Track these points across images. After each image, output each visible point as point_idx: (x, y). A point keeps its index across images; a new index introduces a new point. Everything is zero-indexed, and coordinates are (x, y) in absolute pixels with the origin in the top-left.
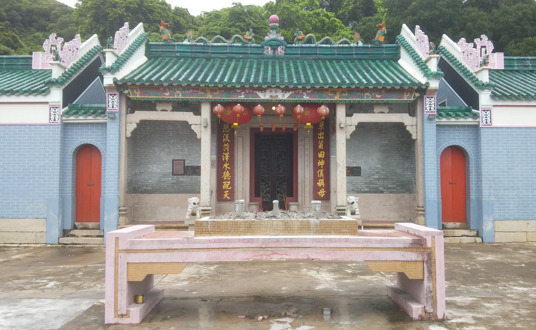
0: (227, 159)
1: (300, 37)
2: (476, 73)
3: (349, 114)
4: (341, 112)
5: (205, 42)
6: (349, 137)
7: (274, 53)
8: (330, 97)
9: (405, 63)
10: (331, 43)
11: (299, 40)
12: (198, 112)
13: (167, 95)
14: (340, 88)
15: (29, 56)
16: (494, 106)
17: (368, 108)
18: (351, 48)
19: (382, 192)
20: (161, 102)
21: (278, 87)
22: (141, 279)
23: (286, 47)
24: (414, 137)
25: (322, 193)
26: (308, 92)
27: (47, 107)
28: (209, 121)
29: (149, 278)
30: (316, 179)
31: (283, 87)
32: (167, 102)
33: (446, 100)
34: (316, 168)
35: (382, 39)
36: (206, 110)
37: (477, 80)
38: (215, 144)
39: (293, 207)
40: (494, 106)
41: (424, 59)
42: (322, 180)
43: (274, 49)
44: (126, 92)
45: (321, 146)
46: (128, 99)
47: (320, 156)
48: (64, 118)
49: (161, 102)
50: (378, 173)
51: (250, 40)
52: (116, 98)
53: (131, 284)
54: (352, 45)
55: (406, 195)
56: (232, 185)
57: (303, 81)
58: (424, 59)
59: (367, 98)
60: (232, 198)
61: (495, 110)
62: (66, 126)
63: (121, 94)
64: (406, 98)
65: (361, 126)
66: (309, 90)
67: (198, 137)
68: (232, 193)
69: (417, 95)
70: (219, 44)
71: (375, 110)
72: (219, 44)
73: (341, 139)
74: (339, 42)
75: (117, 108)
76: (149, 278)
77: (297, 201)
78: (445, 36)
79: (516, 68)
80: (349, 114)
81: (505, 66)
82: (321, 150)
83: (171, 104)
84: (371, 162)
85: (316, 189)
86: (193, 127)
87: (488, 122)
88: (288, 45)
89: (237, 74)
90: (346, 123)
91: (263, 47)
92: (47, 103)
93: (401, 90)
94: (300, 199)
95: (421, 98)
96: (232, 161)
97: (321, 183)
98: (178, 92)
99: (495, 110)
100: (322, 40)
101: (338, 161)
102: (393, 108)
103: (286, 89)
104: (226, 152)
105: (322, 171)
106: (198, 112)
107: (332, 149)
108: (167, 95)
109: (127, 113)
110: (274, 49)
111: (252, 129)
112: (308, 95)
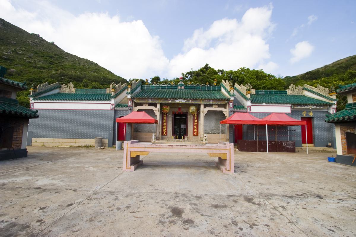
0: (165, 122)
1: (189, 83)
2: (246, 95)
3: (205, 107)
4: (202, 107)
5: (159, 85)
6: (205, 115)
7: (181, 88)
8: (208, 102)
9: (223, 90)
10: (199, 85)
11: (189, 84)
12: (156, 107)
13: (146, 101)
14: (202, 99)
15: (106, 89)
16: (252, 106)
17: (211, 105)
18: (206, 87)
19: (215, 133)
20: (145, 103)
21: (181, 99)
22: (135, 157)
23: (185, 86)
24: (226, 115)
25: (196, 133)
26: (192, 100)
27: (110, 105)
28: (159, 109)
29: (138, 157)
30: (194, 129)
31: (183, 98)
32: (147, 103)
33: (236, 104)
34: (194, 125)
35: (215, 84)
36: (158, 106)
37: (246, 97)
38: (232, 135)
39: (186, 138)
40: (252, 106)
41: (229, 90)
42: (196, 129)
43: (181, 87)
44: (134, 100)
45: (196, 118)
46: (135, 102)
47: (195, 121)
48: (115, 108)
49: (145, 103)
50: (214, 127)
51: (173, 84)
52: (131, 102)
53: (132, 158)
54: (206, 86)
55: (223, 134)
56: (167, 130)
57: (190, 97)
58: (229, 90)
59: (211, 102)
60: (166, 134)
61: (252, 107)
62: (115, 111)
63: (133, 101)
64: (224, 103)
65: (209, 112)
66: (192, 99)
67: (156, 114)
68: (166, 133)
69: (227, 102)
70: (164, 86)
71: (144, 105)
72: (164, 86)
73: (202, 115)
74: (202, 85)
75: (131, 105)
76: (138, 157)
77: (187, 136)
78: (236, 83)
79: (259, 94)
80: (205, 107)
81: (256, 93)
82: (195, 119)
83: (148, 104)
84: (213, 123)
85: (194, 132)
86: (154, 111)
87: (250, 111)
88: (186, 86)
89: (169, 94)
90: (204, 111)
91: (177, 86)
92: (110, 103)
93: (222, 100)
94: (188, 135)
95: (228, 103)
96: (167, 123)
97: (195, 130)
98: (150, 100)
99: (252, 107)
100: (197, 84)
101: (201, 123)
102: (219, 106)
103: (184, 99)
104: (165, 119)
105: (196, 126)
106: (156, 107)
107: (199, 119)
108: (146, 101)
109: (134, 107)
110: (181, 87)
111: (173, 112)
112: (191, 101)
